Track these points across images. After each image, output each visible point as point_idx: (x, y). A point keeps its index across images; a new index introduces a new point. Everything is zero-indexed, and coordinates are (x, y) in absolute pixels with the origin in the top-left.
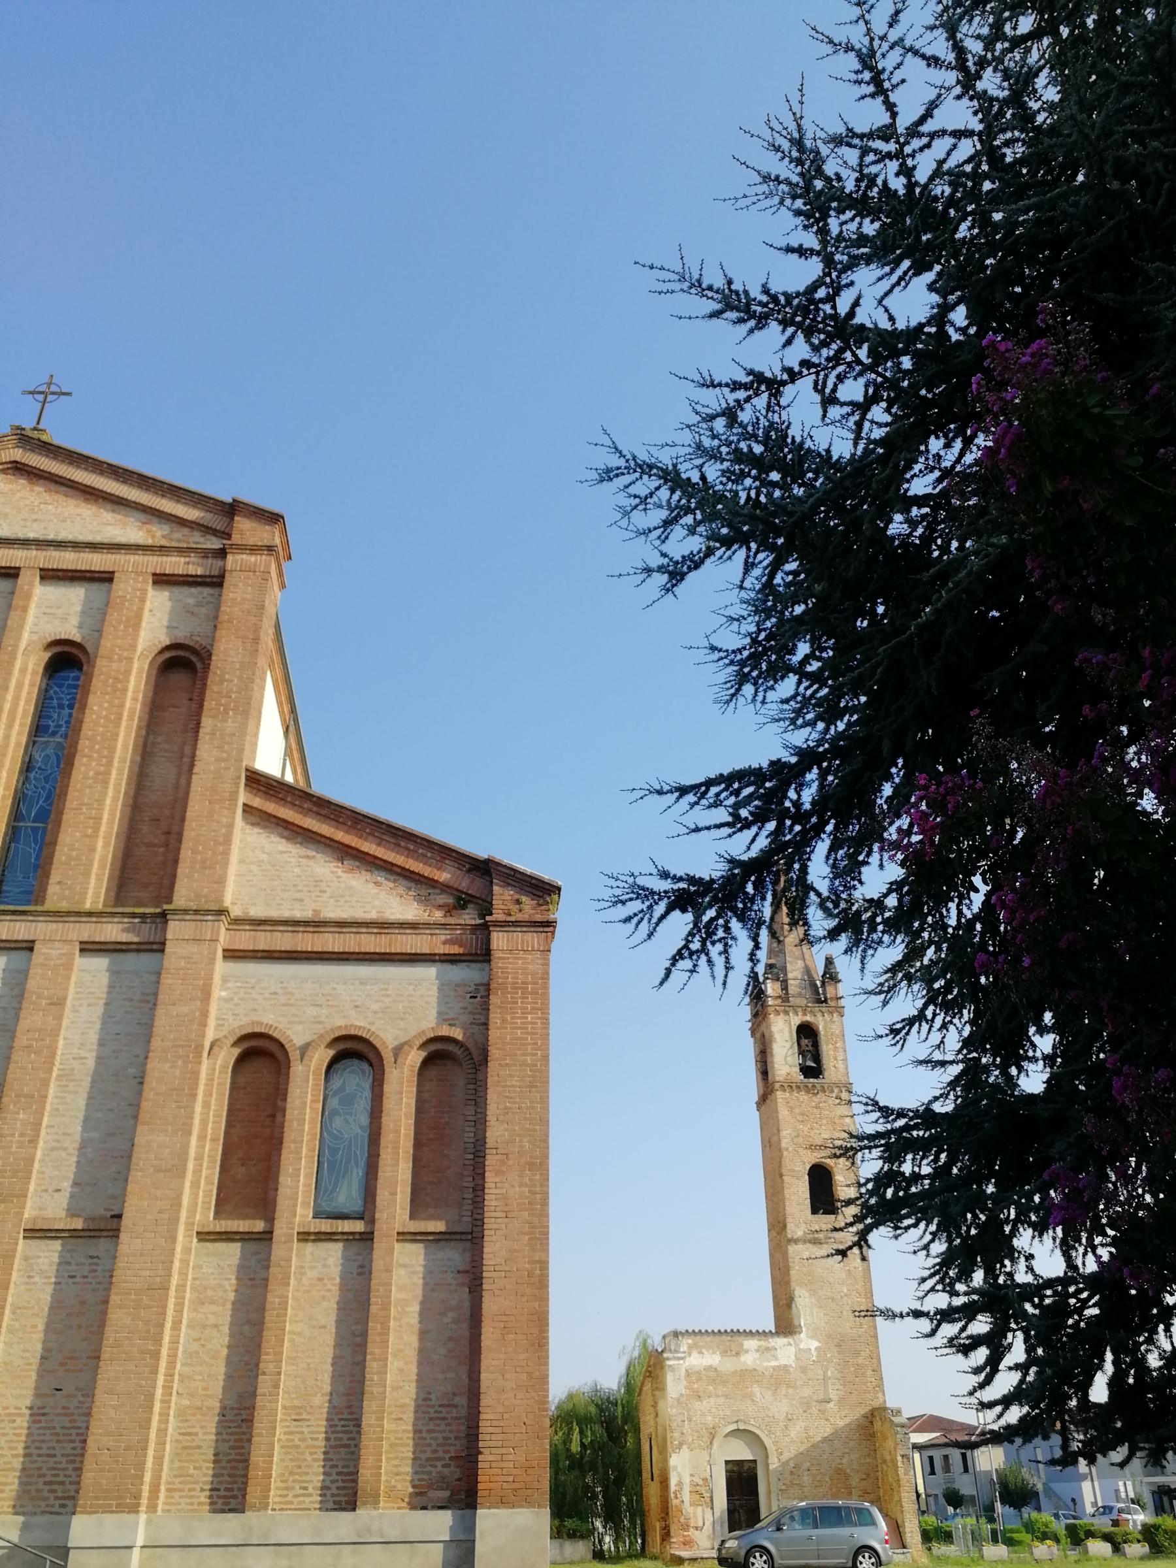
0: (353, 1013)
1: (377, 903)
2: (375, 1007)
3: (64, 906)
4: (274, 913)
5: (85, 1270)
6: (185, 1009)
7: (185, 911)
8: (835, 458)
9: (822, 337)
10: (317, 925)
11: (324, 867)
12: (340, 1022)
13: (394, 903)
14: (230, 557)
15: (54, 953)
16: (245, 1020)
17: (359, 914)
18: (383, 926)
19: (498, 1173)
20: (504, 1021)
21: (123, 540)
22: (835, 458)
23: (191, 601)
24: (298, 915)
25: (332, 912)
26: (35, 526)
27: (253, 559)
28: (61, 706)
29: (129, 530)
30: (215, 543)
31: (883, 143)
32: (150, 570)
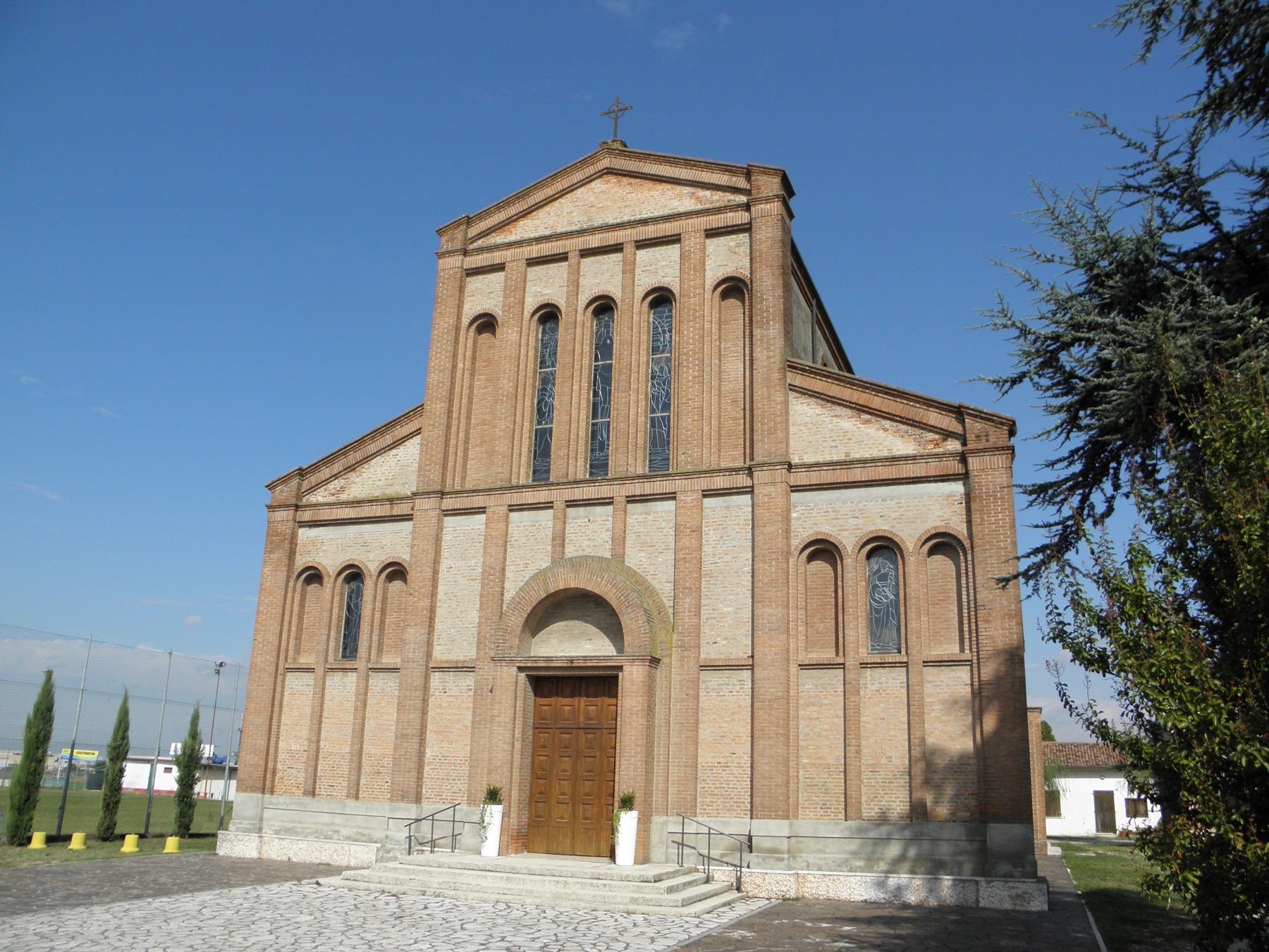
0: (879, 520)
1: (886, 443)
2: (893, 515)
3: (689, 468)
4: (821, 459)
5: (738, 688)
6: (772, 529)
7: (763, 464)
8: (1203, 188)
9: (1111, 283)
10: (848, 464)
11: (847, 422)
12: (872, 528)
13: (898, 442)
14: (753, 208)
15: (689, 499)
16: (811, 532)
17: (875, 453)
18: (893, 460)
19: (987, 621)
20: (982, 519)
21: (682, 210)
22: (1203, 188)
23: (733, 244)
24: (835, 458)
25: (857, 455)
26: (627, 211)
27: (768, 206)
28: (664, 332)
29: (681, 200)
30: (743, 199)
31: (1174, 14)
32: (703, 227)
